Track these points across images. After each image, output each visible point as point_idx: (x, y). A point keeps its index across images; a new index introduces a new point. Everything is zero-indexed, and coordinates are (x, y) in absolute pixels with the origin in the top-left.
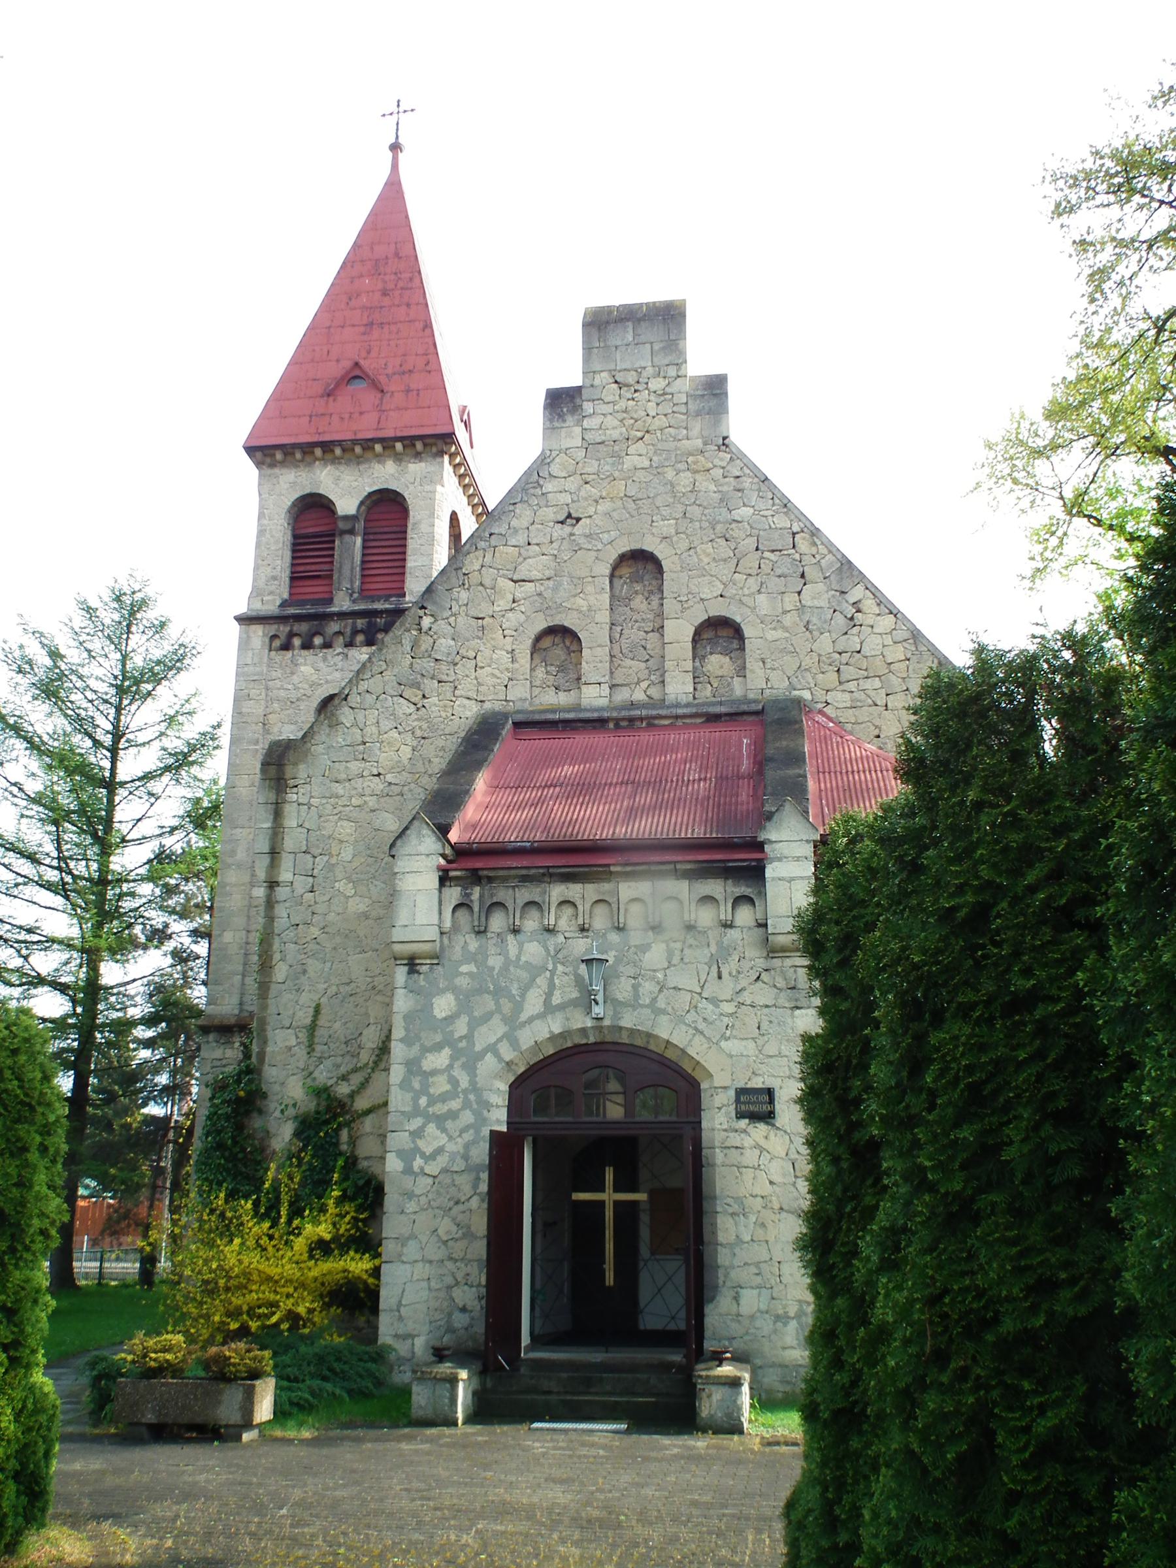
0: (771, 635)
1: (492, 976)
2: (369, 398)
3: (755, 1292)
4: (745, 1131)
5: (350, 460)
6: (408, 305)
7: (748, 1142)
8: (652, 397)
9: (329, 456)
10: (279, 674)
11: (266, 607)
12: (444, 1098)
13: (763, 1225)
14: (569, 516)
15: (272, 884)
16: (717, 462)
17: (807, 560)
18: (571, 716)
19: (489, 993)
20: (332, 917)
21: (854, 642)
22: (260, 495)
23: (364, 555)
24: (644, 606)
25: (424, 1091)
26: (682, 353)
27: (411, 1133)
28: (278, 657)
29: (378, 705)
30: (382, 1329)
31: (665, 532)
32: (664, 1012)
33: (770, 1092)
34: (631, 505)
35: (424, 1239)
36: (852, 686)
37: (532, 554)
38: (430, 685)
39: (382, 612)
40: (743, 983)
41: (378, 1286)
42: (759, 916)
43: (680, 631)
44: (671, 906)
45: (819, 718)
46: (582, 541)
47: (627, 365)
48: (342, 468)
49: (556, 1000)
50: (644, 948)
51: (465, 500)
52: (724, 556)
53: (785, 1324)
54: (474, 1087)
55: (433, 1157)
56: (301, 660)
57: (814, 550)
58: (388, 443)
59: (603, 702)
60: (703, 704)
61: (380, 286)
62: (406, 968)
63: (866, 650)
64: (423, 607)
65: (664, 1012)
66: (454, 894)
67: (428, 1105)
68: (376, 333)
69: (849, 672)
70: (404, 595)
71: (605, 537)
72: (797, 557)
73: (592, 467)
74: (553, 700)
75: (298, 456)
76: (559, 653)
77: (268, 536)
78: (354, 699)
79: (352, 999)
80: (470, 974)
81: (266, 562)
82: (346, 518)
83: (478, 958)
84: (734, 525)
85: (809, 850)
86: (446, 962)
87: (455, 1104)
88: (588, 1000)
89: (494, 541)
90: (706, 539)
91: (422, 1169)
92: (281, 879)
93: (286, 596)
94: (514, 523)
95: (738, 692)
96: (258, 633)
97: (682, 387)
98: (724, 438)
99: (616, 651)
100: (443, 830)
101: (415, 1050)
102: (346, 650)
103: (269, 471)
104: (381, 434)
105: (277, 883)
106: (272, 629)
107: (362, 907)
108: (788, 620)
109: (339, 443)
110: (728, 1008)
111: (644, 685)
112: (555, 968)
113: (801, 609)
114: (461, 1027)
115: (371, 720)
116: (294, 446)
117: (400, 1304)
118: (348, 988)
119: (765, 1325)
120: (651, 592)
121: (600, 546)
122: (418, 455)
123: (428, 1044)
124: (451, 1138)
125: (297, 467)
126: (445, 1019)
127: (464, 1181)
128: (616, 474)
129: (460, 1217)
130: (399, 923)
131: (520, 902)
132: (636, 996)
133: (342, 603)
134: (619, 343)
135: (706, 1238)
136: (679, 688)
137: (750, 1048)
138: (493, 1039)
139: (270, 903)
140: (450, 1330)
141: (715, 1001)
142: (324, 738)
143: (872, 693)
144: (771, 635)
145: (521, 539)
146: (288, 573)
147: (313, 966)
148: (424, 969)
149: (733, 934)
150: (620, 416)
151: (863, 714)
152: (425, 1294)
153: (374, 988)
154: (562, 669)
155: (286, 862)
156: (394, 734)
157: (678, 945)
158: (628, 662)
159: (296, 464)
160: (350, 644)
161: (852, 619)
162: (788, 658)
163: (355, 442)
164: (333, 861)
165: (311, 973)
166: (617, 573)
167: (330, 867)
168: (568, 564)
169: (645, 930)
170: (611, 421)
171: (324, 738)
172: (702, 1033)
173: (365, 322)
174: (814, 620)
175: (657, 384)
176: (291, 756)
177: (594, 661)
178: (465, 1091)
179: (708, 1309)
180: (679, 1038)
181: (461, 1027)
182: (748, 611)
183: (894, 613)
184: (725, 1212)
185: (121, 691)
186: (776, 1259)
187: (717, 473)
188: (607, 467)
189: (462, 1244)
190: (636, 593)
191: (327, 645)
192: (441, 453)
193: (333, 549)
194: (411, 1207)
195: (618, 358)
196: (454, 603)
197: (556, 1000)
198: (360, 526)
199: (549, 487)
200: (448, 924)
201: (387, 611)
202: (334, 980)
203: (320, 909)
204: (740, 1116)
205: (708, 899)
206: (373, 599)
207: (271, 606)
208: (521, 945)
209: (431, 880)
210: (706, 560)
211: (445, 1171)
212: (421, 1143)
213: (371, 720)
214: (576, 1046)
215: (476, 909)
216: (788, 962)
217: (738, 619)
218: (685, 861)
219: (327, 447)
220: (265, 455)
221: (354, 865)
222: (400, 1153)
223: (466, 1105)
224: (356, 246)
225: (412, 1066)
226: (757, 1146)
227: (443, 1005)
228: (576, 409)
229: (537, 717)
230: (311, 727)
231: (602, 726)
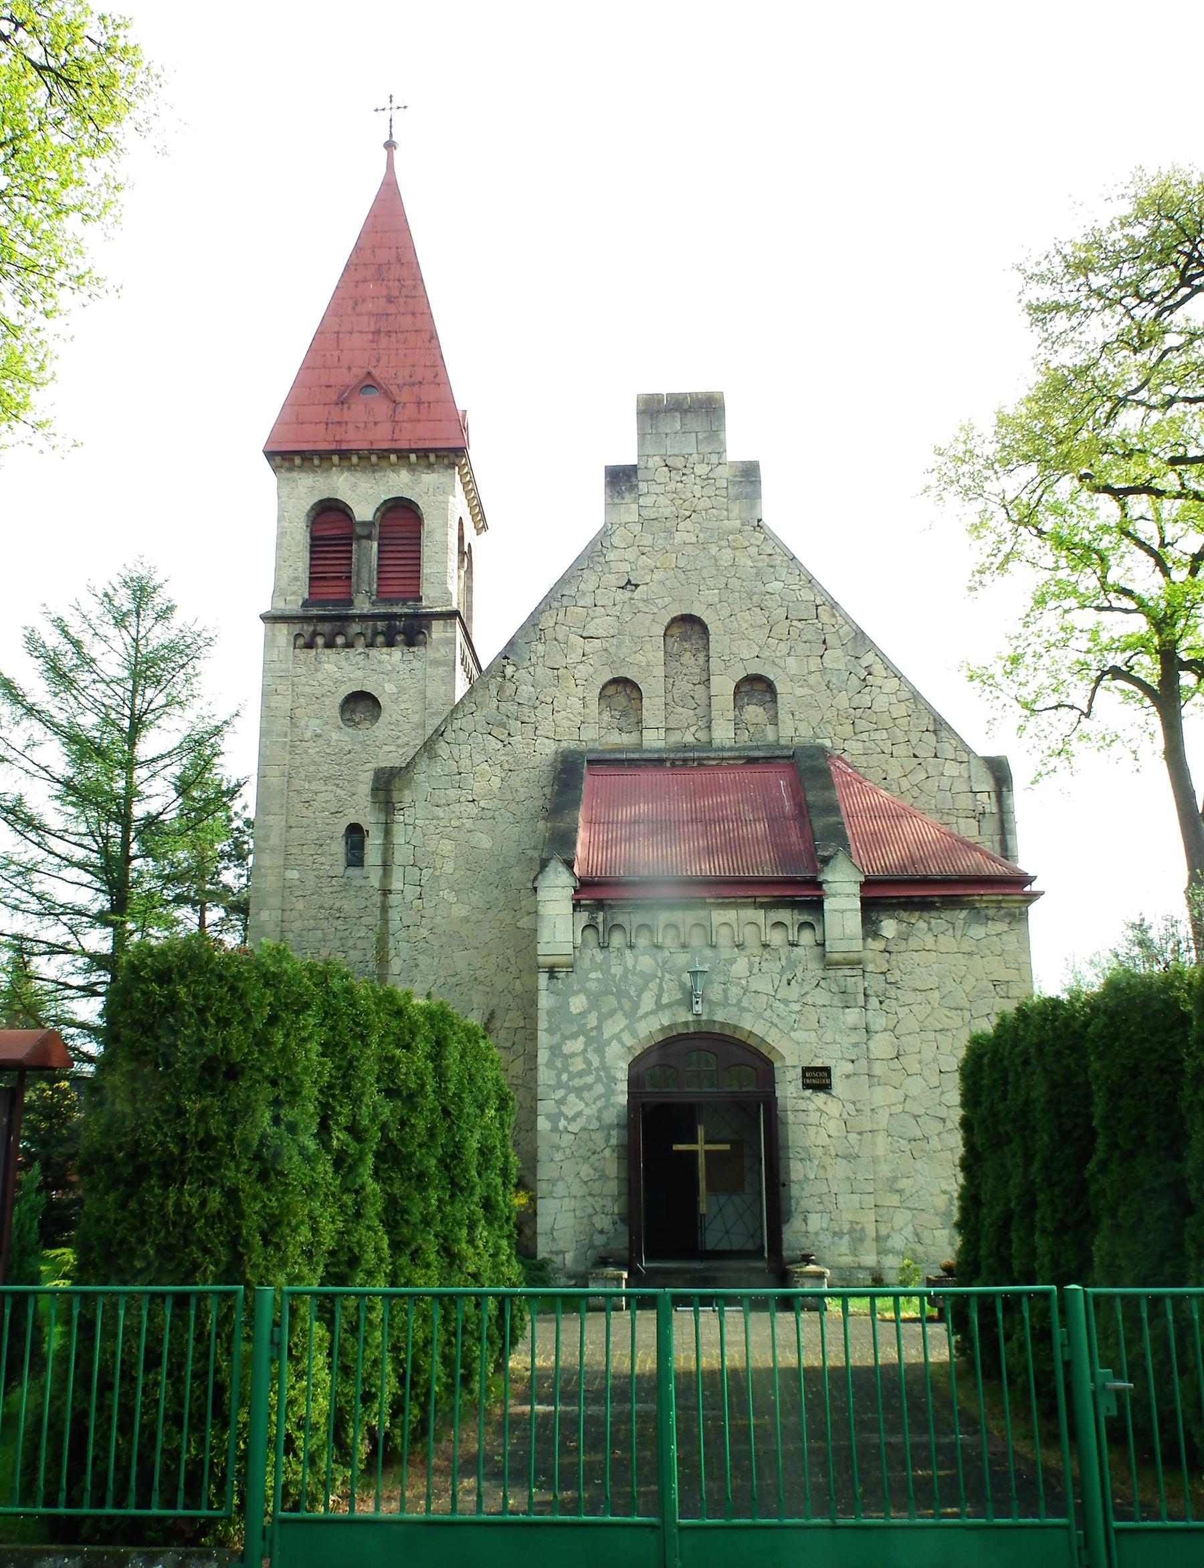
0: (799, 692)
1: (614, 982)
2: (382, 408)
3: (819, 1215)
4: (809, 1099)
5: (365, 468)
6: (413, 314)
7: (812, 1107)
8: (698, 481)
9: (345, 463)
10: (303, 670)
11: (289, 607)
12: (581, 1074)
13: (824, 1167)
14: (629, 582)
15: (386, 892)
16: (753, 541)
17: (828, 628)
18: (636, 756)
19: (612, 994)
20: (438, 920)
21: (866, 700)
22: (279, 497)
23: (379, 558)
24: (692, 662)
25: (565, 1069)
26: (722, 443)
27: (556, 1101)
28: (303, 654)
29: (471, 742)
30: (540, 1248)
31: (710, 600)
33: (827, 1070)
34: (681, 576)
35: (570, 1181)
36: (864, 736)
37: (597, 614)
38: (515, 725)
39: (401, 616)
40: (807, 988)
42: (819, 937)
43: (724, 685)
44: (750, 930)
45: (839, 763)
46: (641, 604)
47: (676, 451)
48: (358, 475)
49: (665, 1000)
50: (732, 961)
51: (466, 502)
53: (840, 1238)
54: (604, 1067)
55: (573, 1119)
56: (325, 658)
57: (833, 621)
58: (402, 454)
59: (661, 744)
60: (745, 748)
61: (385, 292)
63: (875, 708)
64: (506, 658)
66: (583, 917)
67: (569, 1080)
68: (384, 341)
69: (862, 725)
70: (420, 599)
72: (820, 626)
73: (647, 540)
74: (617, 739)
75: (316, 462)
76: (621, 700)
77: (289, 537)
78: (449, 736)
79: (458, 988)
80: (598, 979)
81: (287, 563)
82: (364, 524)
83: (604, 967)
84: (768, 597)
85: (856, 889)
86: (577, 969)
87: (589, 1079)
89: (565, 601)
90: (744, 608)
91: (566, 1128)
92: (393, 888)
93: (306, 596)
94: (582, 586)
95: (771, 736)
96: (283, 632)
97: (723, 473)
98: (759, 521)
99: (669, 700)
100: (569, 865)
101: (557, 1038)
102: (367, 650)
103: (288, 475)
104: (398, 446)
105: (390, 892)
106: (297, 628)
107: (464, 913)
108: (812, 679)
110: (796, 1007)
111: (693, 729)
112: (663, 976)
113: (823, 670)
114: (592, 1020)
115: (465, 754)
116: (314, 453)
117: (553, 1229)
118: (454, 980)
119: (826, 1239)
120: (698, 650)
121: (656, 611)
122: (430, 466)
123: (567, 1033)
124: (587, 1105)
125: (314, 471)
126: (579, 1014)
127: (599, 1138)
128: (668, 548)
129: (597, 1164)
131: (635, 926)
132: (726, 997)
133: (362, 605)
134: (668, 431)
135: (782, 1177)
136: (723, 734)
137: (812, 1036)
138: (617, 1030)
139: (385, 909)
140: (592, 1246)
141: (786, 1002)
142: (424, 768)
143: (881, 743)
144: (799, 692)
145: (588, 601)
146: (307, 574)
147: (423, 960)
151: (874, 760)
152: (571, 1221)
153: (476, 979)
154: (624, 714)
155: (397, 873)
156: (485, 766)
157: (757, 959)
158: (680, 710)
159: (313, 469)
160: (371, 645)
161: (864, 680)
162: (813, 711)
164: (437, 873)
165: (422, 967)
166: (669, 633)
167: (435, 878)
168: (629, 624)
169: (732, 948)
170: (663, 501)
171: (424, 768)
172: (776, 1026)
173: (373, 329)
174: (834, 680)
175: (702, 469)
176: (397, 783)
177: (652, 708)
178: (597, 1069)
179: (785, 1228)
180: (759, 1029)
181: (592, 1020)
183: (898, 676)
184: (796, 1158)
185: (136, 675)
186: (833, 1192)
187: (753, 550)
188: (660, 541)
189: (598, 1184)
190: (685, 650)
191: (349, 645)
192: (452, 465)
194: (558, 1156)
195: (668, 443)
196: (532, 655)
197: (665, 1000)
198: (376, 531)
199: (611, 556)
200: (579, 941)
201: (406, 615)
202: (442, 973)
203: (426, 913)
204: (806, 1086)
205: (778, 924)
206: (392, 602)
207: (294, 606)
208: (636, 958)
210: (745, 626)
211: (584, 1129)
212: (563, 1108)
213: (465, 754)
214: (679, 1035)
215: (601, 929)
216: (840, 973)
217: (772, 677)
218: (764, 894)
219: (344, 455)
220: (283, 459)
221: (457, 876)
222: (549, 1117)
223: (598, 1079)
224: (358, 248)
225: (555, 1050)
226: (819, 1110)
227: (577, 1004)
228: (633, 488)
229: (608, 756)
230: (413, 758)
231: (661, 765)
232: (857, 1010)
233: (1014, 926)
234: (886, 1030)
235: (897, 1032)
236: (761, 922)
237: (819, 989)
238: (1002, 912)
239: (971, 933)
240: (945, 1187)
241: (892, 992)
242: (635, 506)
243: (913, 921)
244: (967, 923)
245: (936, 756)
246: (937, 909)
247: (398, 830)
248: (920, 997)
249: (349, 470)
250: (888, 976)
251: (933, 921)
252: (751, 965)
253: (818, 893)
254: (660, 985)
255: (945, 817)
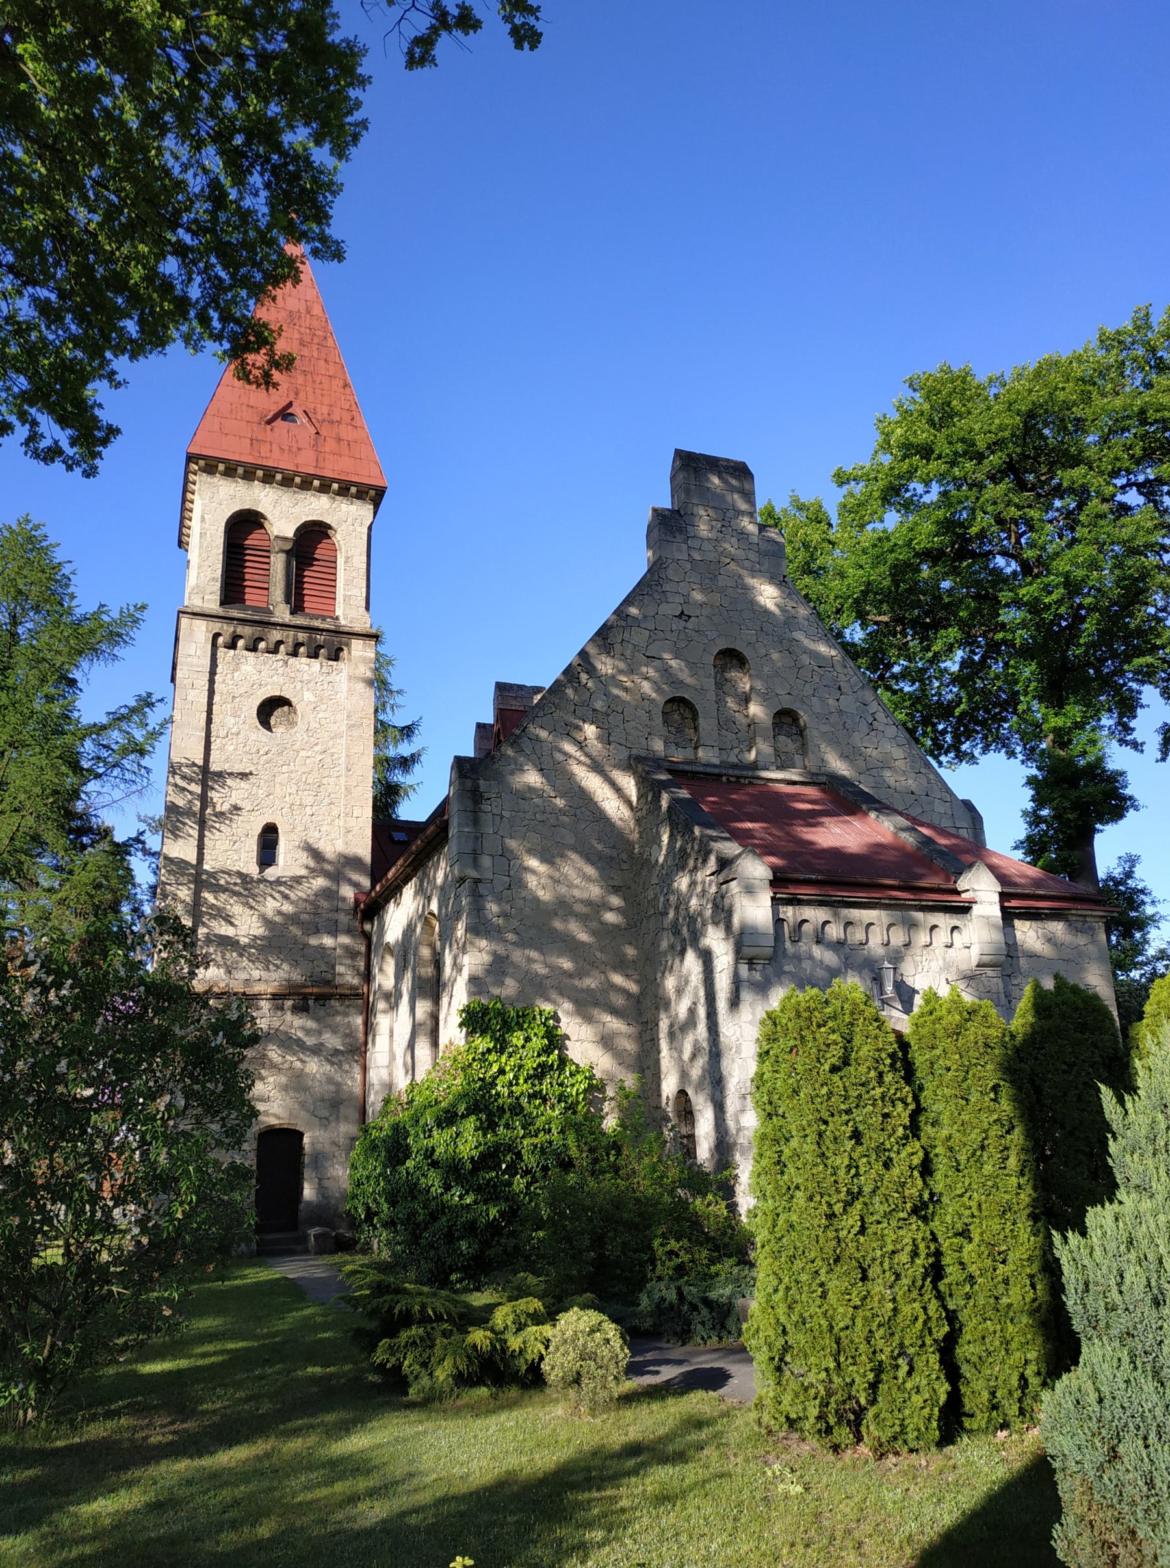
8: (735, 533)
39: (323, 630)
41: (306, 1251)
59: (716, 761)
106: (217, 626)
148: (759, 967)
160: (295, 654)
174: (849, 721)
191: (275, 651)
199: (666, 587)
242: (684, 547)
247: (486, 819)
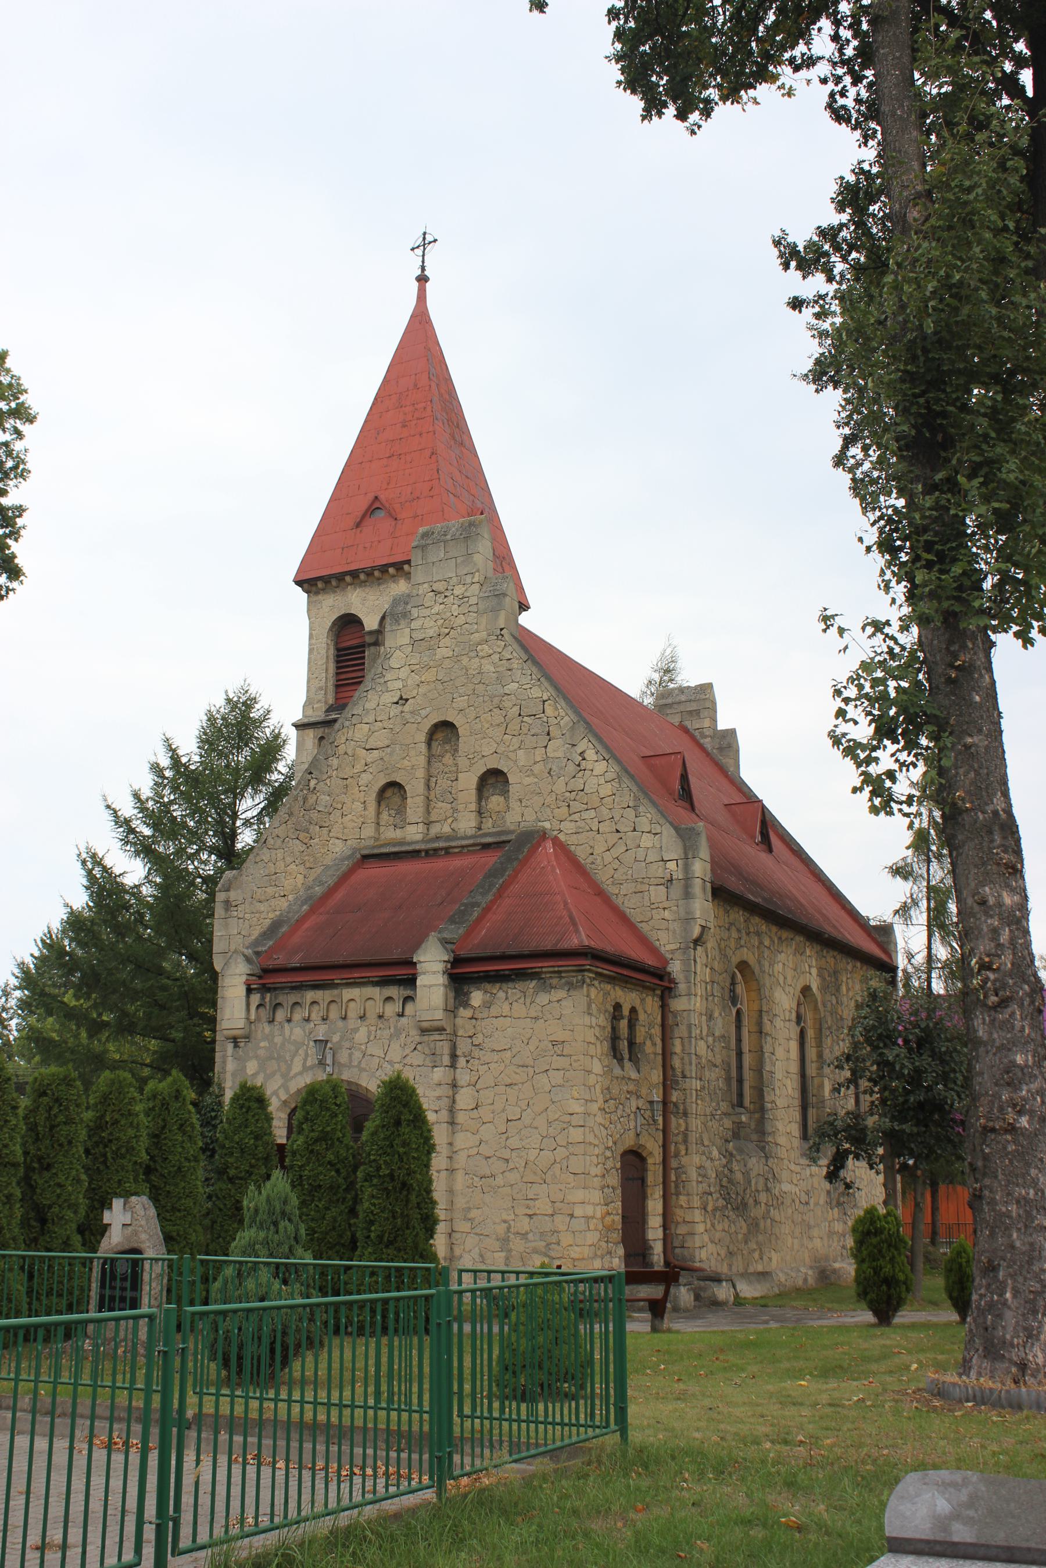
9: (356, 581)
21: (578, 784)
32: (365, 1070)
36: (576, 817)
37: (376, 728)
40: (407, 1051)
43: (469, 781)
46: (408, 716)
48: (367, 590)
49: (309, 1063)
52: (498, 722)
62: (232, 1045)
64: (311, 773)
65: (365, 1070)
69: (576, 806)
71: (423, 713)
72: (545, 719)
82: (371, 633)
83: (269, 1038)
88: (322, 1063)
89: (354, 720)
90: (487, 710)
93: (331, 701)
94: (368, 706)
108: (537, 769)
109: (362, 571)
111: (450, 821)
125: (335, 592)
130: (226, 1017)
131: (291, 1003)
132: (351, 1061)
136: (466, 824)
138: (276, 1087)
143: (589, 822)
144: (527, 781)
148: (242, 1045)
149: (404, 1020)
150: (434, 618)
157: (374, 1028)
158: (440, 804)
161: (579, 765)
163: (373, 568)
166: (434, 737)
174: (554, 768)
175: (459, 591)
182: (511, 763)
187: (496, 657)
190: (446, 751)
193: (364, 658)
200: (253, 1017)
209: (242, 990)
210: (487, 726)
213: (280, 856)
216: (432, 1038)
219: (354, 574)
229: (376, 851)
232: (442, 1069)
233: (572, 992)
234: (469, 1085)
235: (478, 1086)
236: (377, 997)
237: (416, 1052)
238: (563, 981)
239: (538, 1000)
240: (505, 1217)
241: (476, 1053)
243: (495, 991)
244: (536, 993)
245: (635, 830)
246: (513, 980)
248: (496, 1057)
249: (360, 586)
250: (474, 1039)
251: (510, 991)
252: (369, 1033)
253: (412, 972)
254: (307, 1051)
255: (639, 886)
